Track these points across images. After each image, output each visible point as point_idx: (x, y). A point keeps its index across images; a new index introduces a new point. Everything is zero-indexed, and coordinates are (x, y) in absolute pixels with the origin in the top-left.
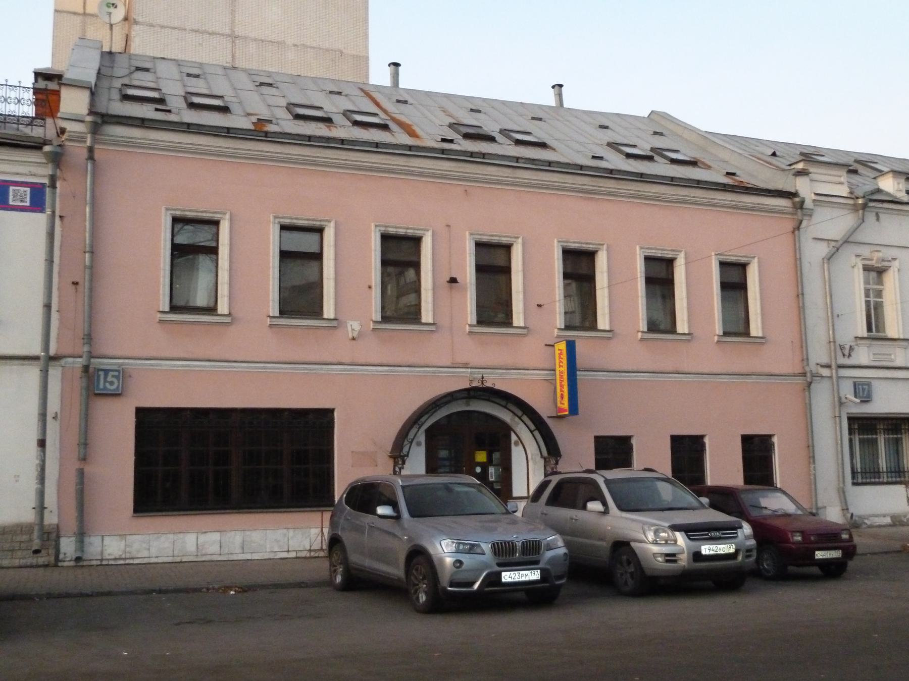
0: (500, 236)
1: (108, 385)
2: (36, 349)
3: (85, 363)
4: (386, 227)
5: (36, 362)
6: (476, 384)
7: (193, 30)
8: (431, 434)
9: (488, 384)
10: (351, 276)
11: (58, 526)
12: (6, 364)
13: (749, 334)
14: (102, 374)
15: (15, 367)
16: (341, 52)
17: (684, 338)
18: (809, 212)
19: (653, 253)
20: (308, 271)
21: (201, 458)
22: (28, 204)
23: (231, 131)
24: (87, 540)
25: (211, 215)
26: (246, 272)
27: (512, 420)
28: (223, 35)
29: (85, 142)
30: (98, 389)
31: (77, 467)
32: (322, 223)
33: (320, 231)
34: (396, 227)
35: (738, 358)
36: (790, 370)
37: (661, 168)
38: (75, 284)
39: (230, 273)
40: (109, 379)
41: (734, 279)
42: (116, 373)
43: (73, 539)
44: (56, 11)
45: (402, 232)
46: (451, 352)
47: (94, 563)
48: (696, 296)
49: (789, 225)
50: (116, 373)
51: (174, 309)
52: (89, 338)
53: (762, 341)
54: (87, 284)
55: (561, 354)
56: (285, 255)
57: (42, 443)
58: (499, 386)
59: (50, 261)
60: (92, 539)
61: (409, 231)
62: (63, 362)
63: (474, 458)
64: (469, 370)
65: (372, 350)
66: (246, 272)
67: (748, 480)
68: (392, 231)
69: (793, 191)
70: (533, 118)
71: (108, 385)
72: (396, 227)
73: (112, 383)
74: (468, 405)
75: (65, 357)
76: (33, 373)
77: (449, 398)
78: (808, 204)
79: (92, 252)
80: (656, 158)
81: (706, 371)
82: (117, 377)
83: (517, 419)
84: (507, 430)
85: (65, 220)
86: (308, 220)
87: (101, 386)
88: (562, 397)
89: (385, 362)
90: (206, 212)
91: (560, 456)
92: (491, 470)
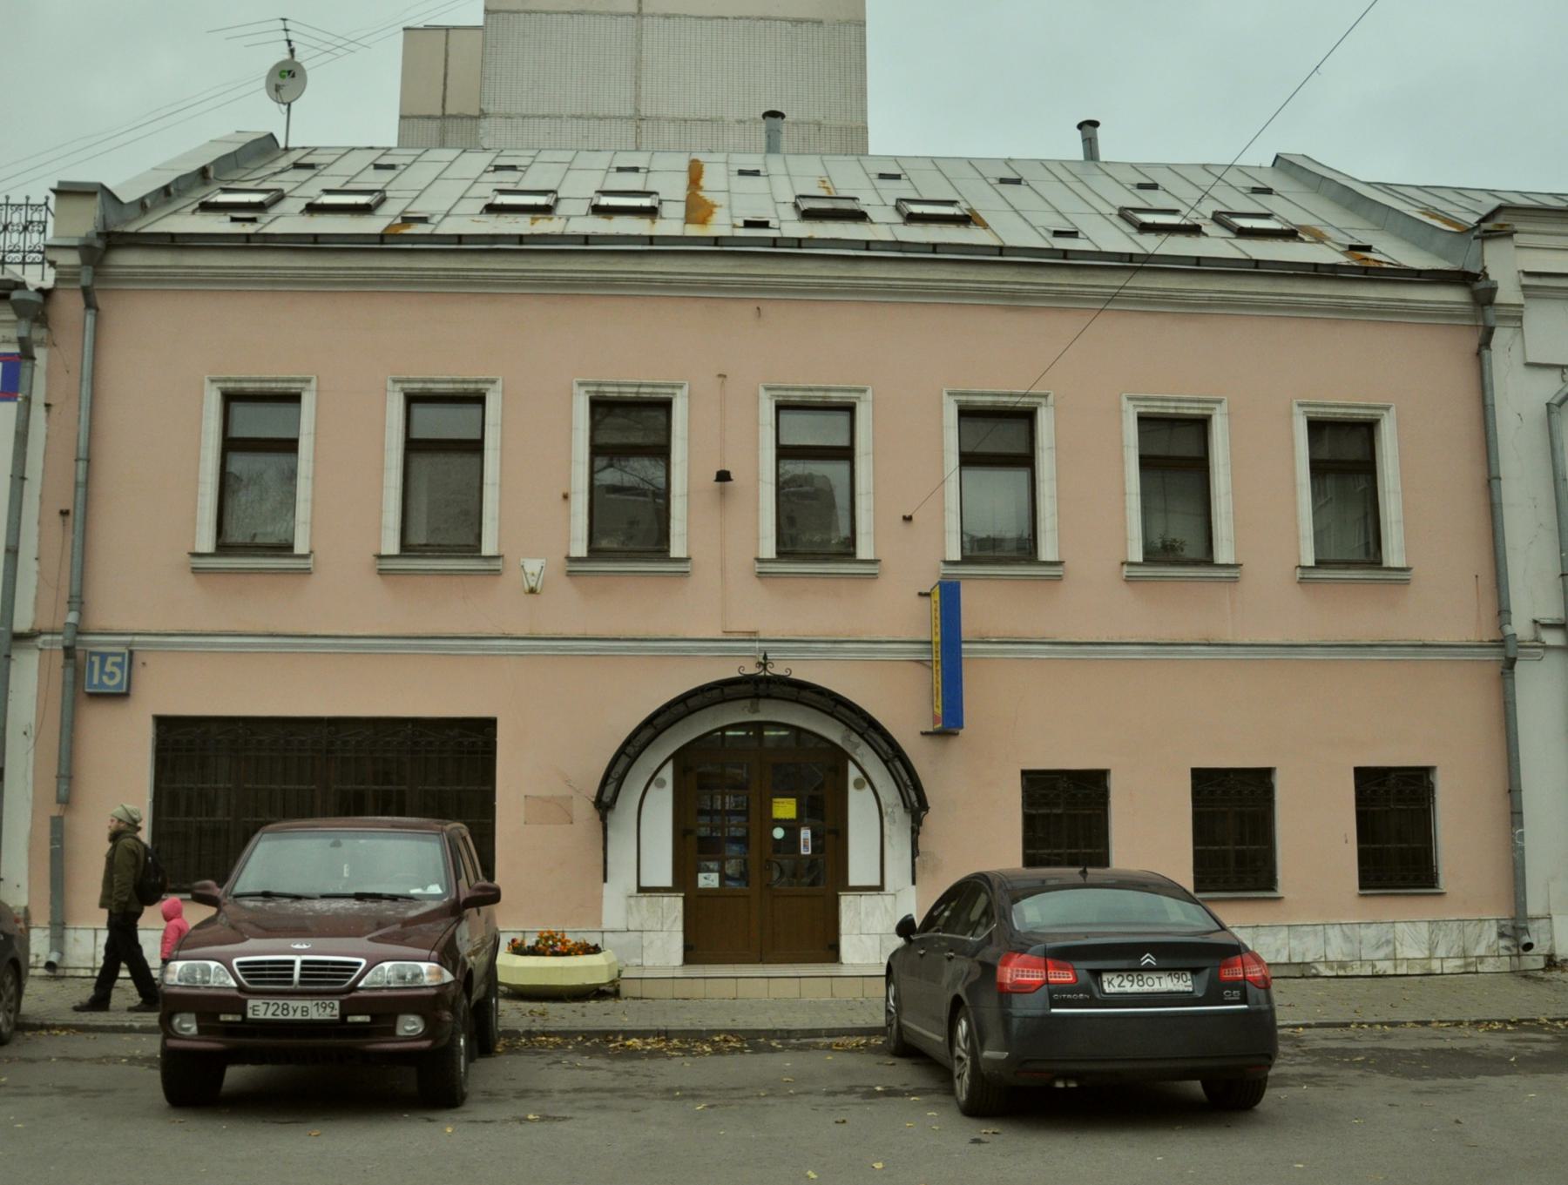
1: (105, 678)
3: (67, 643)
4: (600, 385)
6: (751, 669)
7: (573, 117)
8: (681, 759)
9: (777, 669)
11: (26, 910)
13: (1380, 563)
14: (96, 659)
16: (819, 124)
18: (1513, 311)
19: (1156, 408)
20: (641, 470)
24: (70, 935)
25: (285, 385)
26: (348, 483)
27: (846, 738)
28: (621, 118)
29: (78, 281)
30: (91, 685)
31: (55, 814)
32: (480, 386)
33: (479, 399)
34: (618, 385)
35: (1354, 613)
36: (1473, 638)
38: (64, 513)
40: (108, 668)
41: (1344, 455)
42: (119, 659)
43: (47, 932)
44: (402, 117)
45: (629, 392)
46: (724, 601)
47: (82, 973)
48: (1262, 494)
49: (1472, 342)
50: (119, 659)
51: (224, 547)
52: (78, 601)
54: (79, 513)
58: (800, 674)
60: (81, 934)
61: (642, 390)
62: (40, 641)
63: (771, 813)
64: (757, 645)
65: (572, 610)
66: (348, 483)
68: (612, 392)
69: (1477, 270)
71: (105, 678)
72: (618, 385)
73: (112, 675)
74: (756, 711)
75: (41, 633)
78: (1508, 292)
79: (88, 461)
81: (1247, 641)
82: (120, 666)
83: (855, 738)
84: (838, 759)
85: (53, 409)
86: (448, 382)
87: (96, 681)
89: (591, 633)
90: (276, 381)
92: (805, 834)
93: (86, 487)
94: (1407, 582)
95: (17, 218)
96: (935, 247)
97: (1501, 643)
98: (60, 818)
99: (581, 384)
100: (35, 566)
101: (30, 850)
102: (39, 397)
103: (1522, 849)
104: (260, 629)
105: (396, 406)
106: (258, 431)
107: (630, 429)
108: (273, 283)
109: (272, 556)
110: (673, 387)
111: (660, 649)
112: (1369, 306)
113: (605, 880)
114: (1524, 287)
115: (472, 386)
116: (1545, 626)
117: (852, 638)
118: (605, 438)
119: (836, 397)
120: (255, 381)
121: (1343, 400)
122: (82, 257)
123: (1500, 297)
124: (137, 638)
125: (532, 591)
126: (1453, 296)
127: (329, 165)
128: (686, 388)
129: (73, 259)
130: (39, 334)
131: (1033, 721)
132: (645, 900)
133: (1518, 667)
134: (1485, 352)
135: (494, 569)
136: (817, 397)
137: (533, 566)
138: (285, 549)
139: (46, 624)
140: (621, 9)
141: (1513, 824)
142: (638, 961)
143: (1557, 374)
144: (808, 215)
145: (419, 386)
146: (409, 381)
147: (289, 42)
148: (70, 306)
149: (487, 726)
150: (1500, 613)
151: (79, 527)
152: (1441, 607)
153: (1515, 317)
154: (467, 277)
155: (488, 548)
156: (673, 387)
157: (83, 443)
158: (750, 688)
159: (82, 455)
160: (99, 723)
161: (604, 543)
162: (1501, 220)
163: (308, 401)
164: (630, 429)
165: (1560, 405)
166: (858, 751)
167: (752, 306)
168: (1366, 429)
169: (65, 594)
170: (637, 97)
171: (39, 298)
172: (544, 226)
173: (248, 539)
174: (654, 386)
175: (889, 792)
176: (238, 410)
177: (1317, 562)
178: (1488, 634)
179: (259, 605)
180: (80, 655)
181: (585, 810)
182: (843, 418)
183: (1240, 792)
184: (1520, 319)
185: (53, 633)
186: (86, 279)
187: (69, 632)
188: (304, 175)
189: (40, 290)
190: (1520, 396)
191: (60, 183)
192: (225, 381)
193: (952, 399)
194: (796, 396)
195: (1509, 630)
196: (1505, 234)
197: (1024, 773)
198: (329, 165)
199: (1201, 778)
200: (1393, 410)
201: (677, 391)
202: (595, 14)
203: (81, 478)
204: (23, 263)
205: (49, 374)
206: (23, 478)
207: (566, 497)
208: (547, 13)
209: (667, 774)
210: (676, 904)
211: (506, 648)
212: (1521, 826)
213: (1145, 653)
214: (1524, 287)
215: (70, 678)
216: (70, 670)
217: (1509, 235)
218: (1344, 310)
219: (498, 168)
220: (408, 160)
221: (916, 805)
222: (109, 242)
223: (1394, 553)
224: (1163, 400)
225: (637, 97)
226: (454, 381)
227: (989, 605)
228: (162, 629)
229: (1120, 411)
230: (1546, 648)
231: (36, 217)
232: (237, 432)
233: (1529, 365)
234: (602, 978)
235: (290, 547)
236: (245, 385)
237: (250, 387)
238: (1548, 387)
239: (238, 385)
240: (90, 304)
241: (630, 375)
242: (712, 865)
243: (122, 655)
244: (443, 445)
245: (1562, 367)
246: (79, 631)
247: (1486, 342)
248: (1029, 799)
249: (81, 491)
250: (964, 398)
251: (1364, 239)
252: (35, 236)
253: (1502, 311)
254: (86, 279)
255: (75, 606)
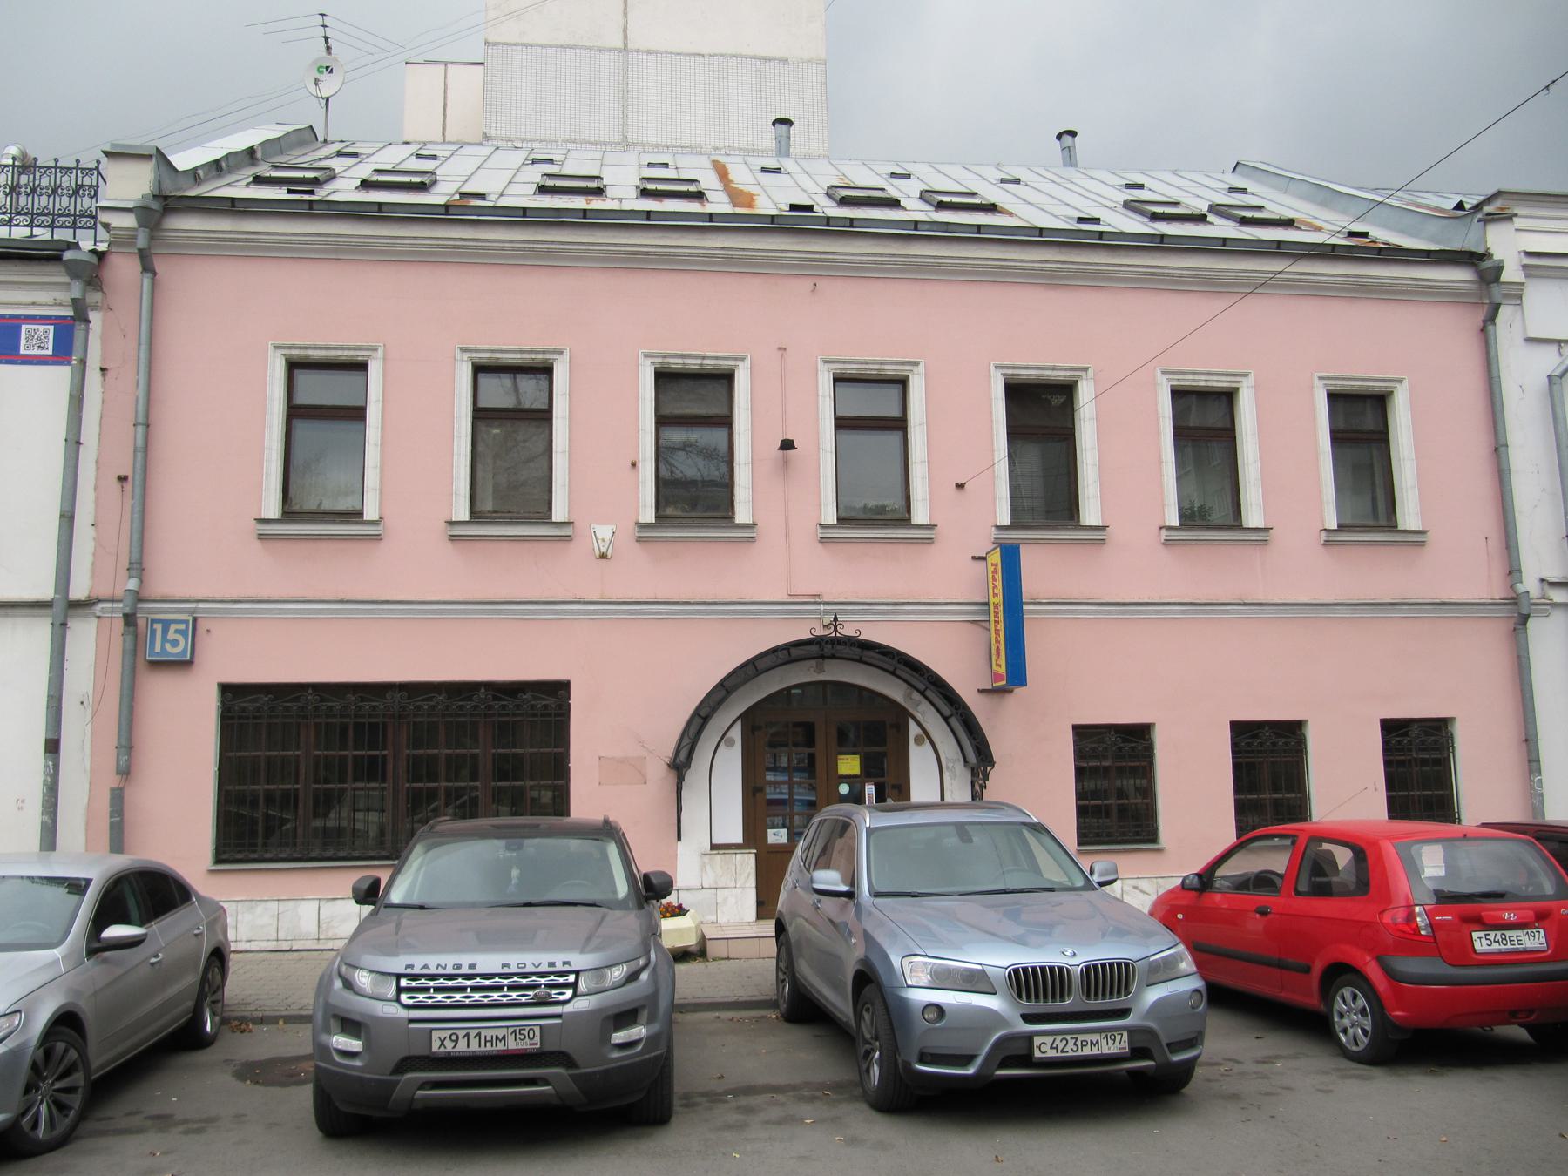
0: (881, 363)
1: (168, 646)
2: (47, 592)
3: (127, 610)
5: (48, 611)
8: (750, 720)
9: (848, 631)
10: (604, 449)
12: (7, 615)
15: (20, 621)
17: (1416, 538)
18: (1514, 290)
19: (1187, 382)
21: (338, 768)
22: (50, 352)
23: (384, 209)
26: (417, 449)
27: (908, 696)
29: (133, 244)
30: (152, 653)
31: (115, 785)
32: (548, 356)
35: (1373, 574)
37: (1221, 228)
38: (122, 479)
39: (382, 451)
40: (171, 635)
41: (1360, 422)
42: (182, 627)
45: (693, 364)
46: (788, 567)
48: (1287, 460)
49: (1481, 314)
50: (182, 627)
51: (290, 513)
52: (138, 567)
53: (1417, 538)
54: (138, 478)
55: (994, 572)
56: (481, 415)
57: (53, 746)
58: (869, 634)
59: (74, 442)
66: (417, 449)
67: (1398, 808)
68: (676, 364)
69: (1481, 250)
70: (1003, 181)
71: (168, 646)
73: (175, 643)
74: (820, 670)
75: (100, 601)
76: (39, 632)
77: (782, 655)
78: (1511, 274)
80: (1211, 218)
82: (183, 633)
83: (916, 695)
84: (901, 717)
85: (109, 374)
87: (158, 649)
88: (998, 654)
89: (661, 597)
90: (342, 348)
91: (992, 764)
93: (145, 451)
94: (1422, 544)
95: (67, 181)
96: (979, 228)
97: (1514, 600)
98: (121, 790)
99: (646, 356)
100: (91, 532)
101: (87, 824)
102: (94, 361)
103: (1541, 795)
104: (329, 597)
105: (465, 374)
106: (324, 402)
107: (693, 398)
108: (336, 252)
109: (342, 522)
110: (736, 359)
111: (728, 612)
112: (1382, 285)
113: (679, 838)
114: (1525, 267)
115: (540, 356)
116: (1553, 584)
117: (918, 601)
118: (667, 411)
119: (890, 370)
120: (320, 348)
121: (1360, 373)
122: (138, 220)
123: (1504, 277)
124: (201, 605)
125: (603, 556)
126: (1461, 275)
127: (369, 156)
128: (748, 361)
129: (129, 221)
130: (94, 297)
131: (1083, 677)
132: (718, 858)
133: (1531, 623)
134: (1490, 327)
135: (565, 534)
136: (872, 369)
137: (604, 532)
138: (355, 516)
139: (104, 591)
140: (613, 45)
141: (1531, 772)
142: (713, 918)
143: (1554, 348)
144: (844, 202)
145: (487, 355)
146: (477, 351)
147: (326, 39)
148: (124, 269)
149: (558, 691)
150: (1510, 573)
151: (138, 491)
152: (1458, 567)
153: (1516, 295)
154: (533, 249)
155: (559, 513)
156: (736, 359)
157: (141, 408)
158: (814, 649)
159: (141, 419)
160: (161, 692)
161: (669, 511)
162: (1494, 209)
163: (375, 369)
164: (693, 398)
165: (1561, 376)
166: (920, 708)
167: (808, 284)
168: (1379, 401)
169: (124, 562)
170: (625, 124)
171: (94, 260)
172: (596, 204)
173: (312, 504)
174: (717, 358)
175: (948, 748)
176: (302, 377)
177: (1339, 526)
178: (1497, 592)
179: (324, 570)
180: (141, 623)
181: (658, 770)
182: (894, 391)
183: (1274, 744)
184: (1520, 297)
185: (113, 601)
186: (142, 242)
187: (129, 600)
188: (350, 161)
189: (94, 252)
190: (1524, 372)
191: (113, 145)
192: (290, 348)
193: (999, 372)
194: (852, 369)
195: (1521, 588)
196: (1504, 217)
197: (1075, 727)
198: (369, 156)
199: (1235, 726)
200: (1406, 383)
201: (740, 364)
202: (585, 48)
203: (140, 443)
204: (74, 227)
205: (105, 340)
206: (78, 443)
207: (634, 465)
208: (542, 46)
209: (736, 733)
210: (746, 862)
211: (579, 612)
212: (1540, 773)
213: (1182, 612)
214: (1525, 267)
215: (129, 645)
216: (129, 638)
217: (1510, 218)
218: (1359, 291)
219: (535, 161)
220: (447, 154)
221: (980, 758)
222: (167, 202)
223: (1409, 518)
224: (1194, 373)
225: (625, 124)
226: (522, 352)
227: (1047, 568)
228: (227, 596)
229: (1156, 384)
230: (1555, 605)
231: (87, 181)
232: (301, 399)
233: (1529, 340)
234: (690, 941)
235: (360, 514)
236: (310, 352)
237: (316, 354)
238: (1549, 360)
239: (302, 352)
240: (148, 268)
241: (694, 347)
242: (779, 820)
243: (186, 622)
244: (512, 417)
245: (1559, 342)
246: (138, 597)
247: (1491, 318)
248: (1079, 754)
249: (140, 456)
250: (1010, 372)
251: (1358, 227)
252: (87, 200)
253: (1505, 290)
254: (142, 242)
255: (134, 572)
